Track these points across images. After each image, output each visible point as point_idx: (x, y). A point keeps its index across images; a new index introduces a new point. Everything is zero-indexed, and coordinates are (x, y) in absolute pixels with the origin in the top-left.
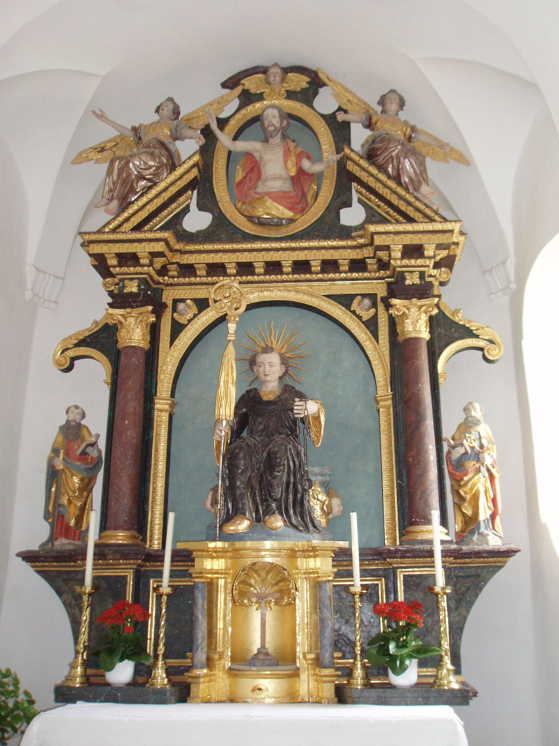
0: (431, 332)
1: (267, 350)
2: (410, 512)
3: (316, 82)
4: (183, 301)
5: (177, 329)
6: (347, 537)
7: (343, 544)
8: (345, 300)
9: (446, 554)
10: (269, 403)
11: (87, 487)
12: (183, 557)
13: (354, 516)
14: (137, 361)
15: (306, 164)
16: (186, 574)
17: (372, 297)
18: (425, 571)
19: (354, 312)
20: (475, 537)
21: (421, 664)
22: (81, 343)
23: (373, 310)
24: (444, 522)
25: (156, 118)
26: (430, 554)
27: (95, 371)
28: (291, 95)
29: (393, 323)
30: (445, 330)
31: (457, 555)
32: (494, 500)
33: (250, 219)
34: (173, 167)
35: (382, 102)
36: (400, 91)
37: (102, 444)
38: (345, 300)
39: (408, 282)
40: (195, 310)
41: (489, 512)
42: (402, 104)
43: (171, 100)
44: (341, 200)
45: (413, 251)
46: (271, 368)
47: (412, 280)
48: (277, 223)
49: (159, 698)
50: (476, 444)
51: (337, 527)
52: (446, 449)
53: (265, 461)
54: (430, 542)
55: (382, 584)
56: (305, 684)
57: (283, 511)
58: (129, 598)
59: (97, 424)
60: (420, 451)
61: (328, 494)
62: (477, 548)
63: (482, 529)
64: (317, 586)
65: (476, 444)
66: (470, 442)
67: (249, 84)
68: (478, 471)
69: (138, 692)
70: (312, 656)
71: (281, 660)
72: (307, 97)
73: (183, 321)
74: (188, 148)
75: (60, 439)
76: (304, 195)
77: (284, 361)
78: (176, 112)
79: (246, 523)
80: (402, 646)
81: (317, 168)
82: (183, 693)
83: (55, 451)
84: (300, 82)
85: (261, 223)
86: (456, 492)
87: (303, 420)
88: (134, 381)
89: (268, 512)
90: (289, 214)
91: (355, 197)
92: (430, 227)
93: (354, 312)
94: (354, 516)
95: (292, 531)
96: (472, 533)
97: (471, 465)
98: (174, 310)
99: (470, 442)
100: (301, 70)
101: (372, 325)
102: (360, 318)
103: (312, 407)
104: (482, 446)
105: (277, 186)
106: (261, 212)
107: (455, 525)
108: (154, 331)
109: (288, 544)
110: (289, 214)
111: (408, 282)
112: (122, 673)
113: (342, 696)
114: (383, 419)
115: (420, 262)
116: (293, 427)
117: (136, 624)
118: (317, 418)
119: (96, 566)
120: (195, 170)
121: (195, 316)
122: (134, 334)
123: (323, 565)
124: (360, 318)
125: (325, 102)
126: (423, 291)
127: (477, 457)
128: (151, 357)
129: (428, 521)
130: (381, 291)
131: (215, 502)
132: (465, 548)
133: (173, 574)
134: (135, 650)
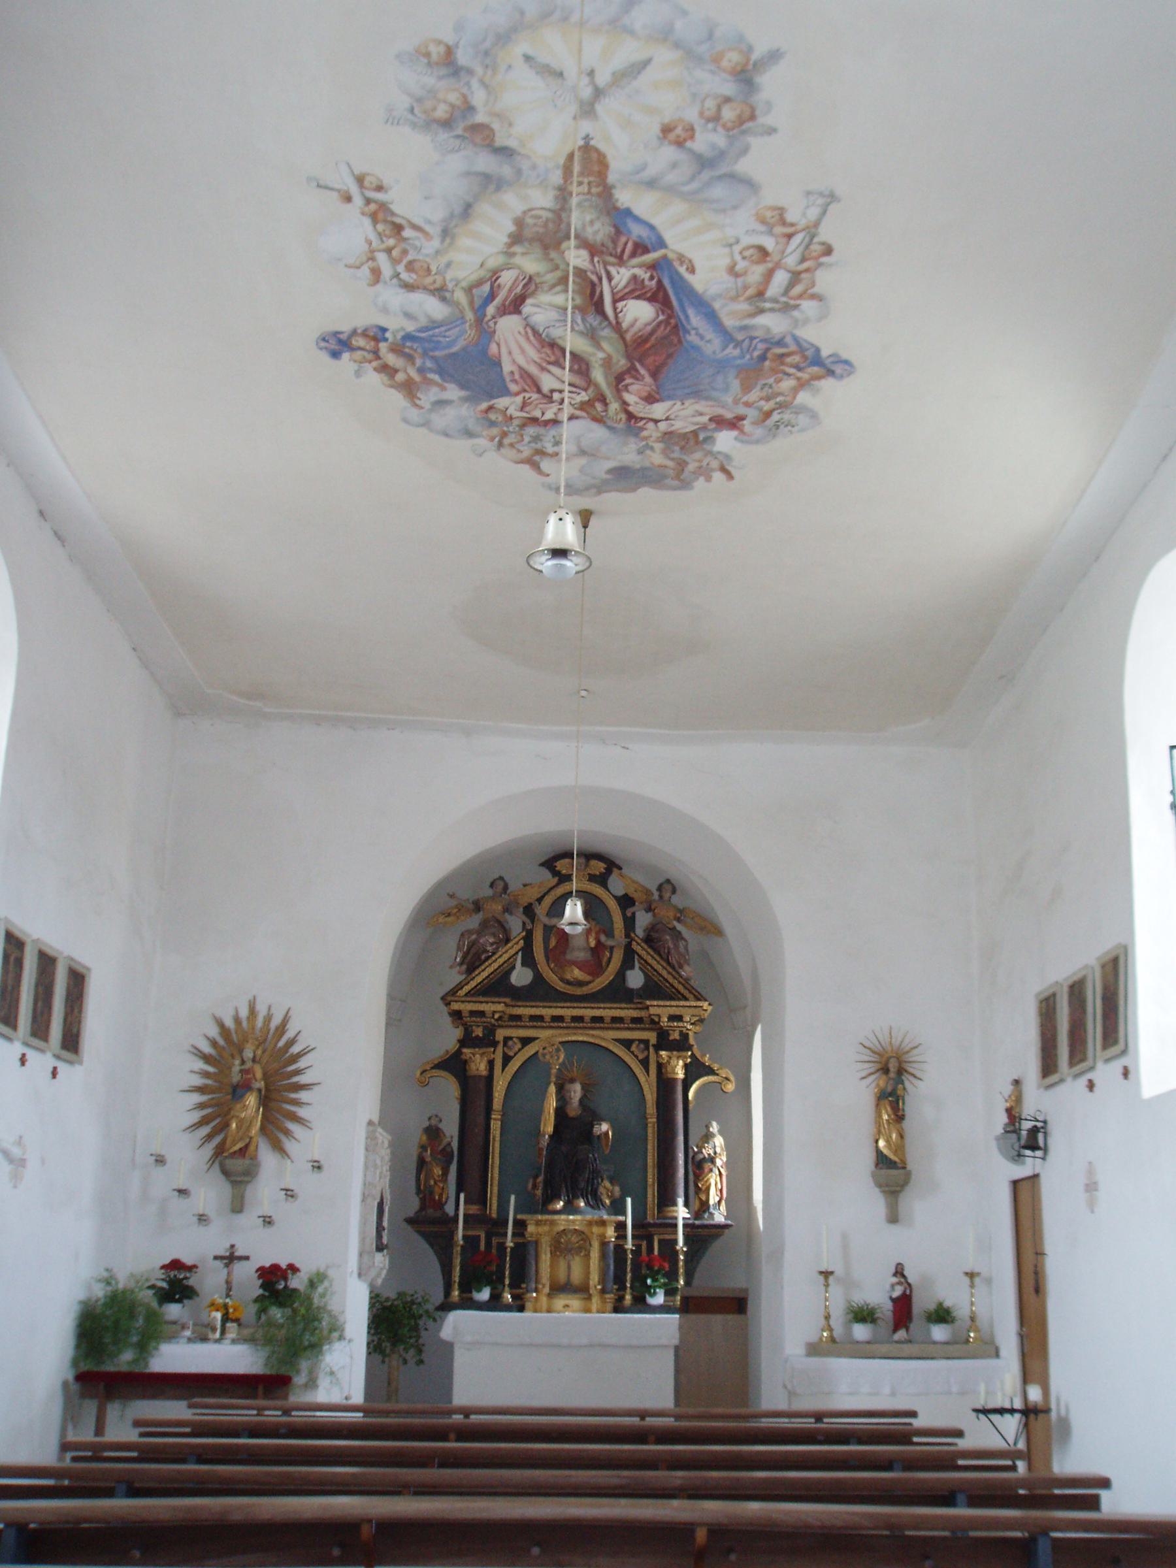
0: (686, 1074)
1: (572, 1081)
2: (666, 1199)
3: (612, 865)
4: (511, 1038)
5: (507, 1059)
6: (624, 1213)
7: (621, 1218)
8: (627, 1044)
9: (685, 1226)
10: (573, 1119)
11: (445, 1172)
12: (520, 1225)
13: (629, 1200)
14: (482, 1085)
15: (603, 938)
16: (523, 1235)
17: (646, 1042)
18: (672, 1237)
19: (632, 1053)
20: (706, 1215)
21: (666, 1294)
22: (438, 1066)
23: (646, 1053)
24: (686, 1205)
25: (490, 892)
26: (676, 1226)
27: (449, 1087)
28: (592, 878)
29: (660, 1066)
30: (696, 1070)
31: (692, 1226)
32: (721, 1191)
33: (562, 980)
34: (508, 940)
35: (660, 888)
36: (673, 882)
37: (455, 1145)
38: (627, 1044)
39: (671, 1038)
40: (519, 1046)
41: (717, 1199)
42: (674, 891)
43: (501, 878)
44: (628, 961)
45: (672, 1018)
46: (576, 1091)
47: (675, 1035)
48: (580, 984)
49: (508, 1308)
50: (711, 1152)
51: (618, 1207)
52: (691, 1154)
53: (570, 1165)
54: (676, 1218)
55: (644, 1244)
56: (596, 1302)
57: (585, 1197)
58: (482, 1247)
59: (451, 1129)
60: (673, 1159)
61: (612, 1183)
62: (706, 1222)
63: (711, 1210)
64: (604, 1244)
65: (711, 1152)
66: (707, 1151)
67: (561, 865)
68: (711, 1170)
69: (495, 1304)
70: (599, 1287)
71: (582, 1290)
72: (601, 880)
73: (511, 1054)
74: (515, 924)
75: (424, 1138)
76: (600, 962)
77: (585, 1088)
78: (506, 887)
79: (562, 1203)
80: (655, 1280)
81: (610, 943)
82: (521, 1309)
83: (423, 1148)
84: (598, 867)
85: (568, 983)
86: (696, 1186)
87: (599, 1137)
88: (474, 1094)
89: (576, 1197)
90: (588, 978)
91: (637, 965)
92: (687, 1003)
93: (632, 1053)
94: (629, 1200)
95: (589, 1209)
96: (704, 1212)
97: (708, 1165)
98: (505, 1044)
99: (707, 1151)
100: (599, 857)
101: (645, 1063)
102: (636, 1057)
103: (605, 1127)
104: (715, 1153)
105: (581, 955)
106: (568, 977)
107: (696, 1205)
108: (491, 1063)
109: (589, 1217)
110: (588, 978)
111: (671, 1038)
112: (484, 1295)
113: (617, 1309)
114: (650, 1130)
115: (681, 1024)
116: (587, 1136)
117: (498, 1266)
118: (607, 1133)
119: (464, 1228)
120: (522, 942)
121: (520, 1050)
122: (478, 1065)
123: (611, 1233)
124: (636, 1057)
125: (617, 885)
126: (682, 1045)
127: (712, 1160)
128: (489, 1079)
129: (675, 1204)
130: (653, 1041)
131: (535, 1186)
132: (697, 1222)
133: (514, 1234)
134: (496, 1283)
